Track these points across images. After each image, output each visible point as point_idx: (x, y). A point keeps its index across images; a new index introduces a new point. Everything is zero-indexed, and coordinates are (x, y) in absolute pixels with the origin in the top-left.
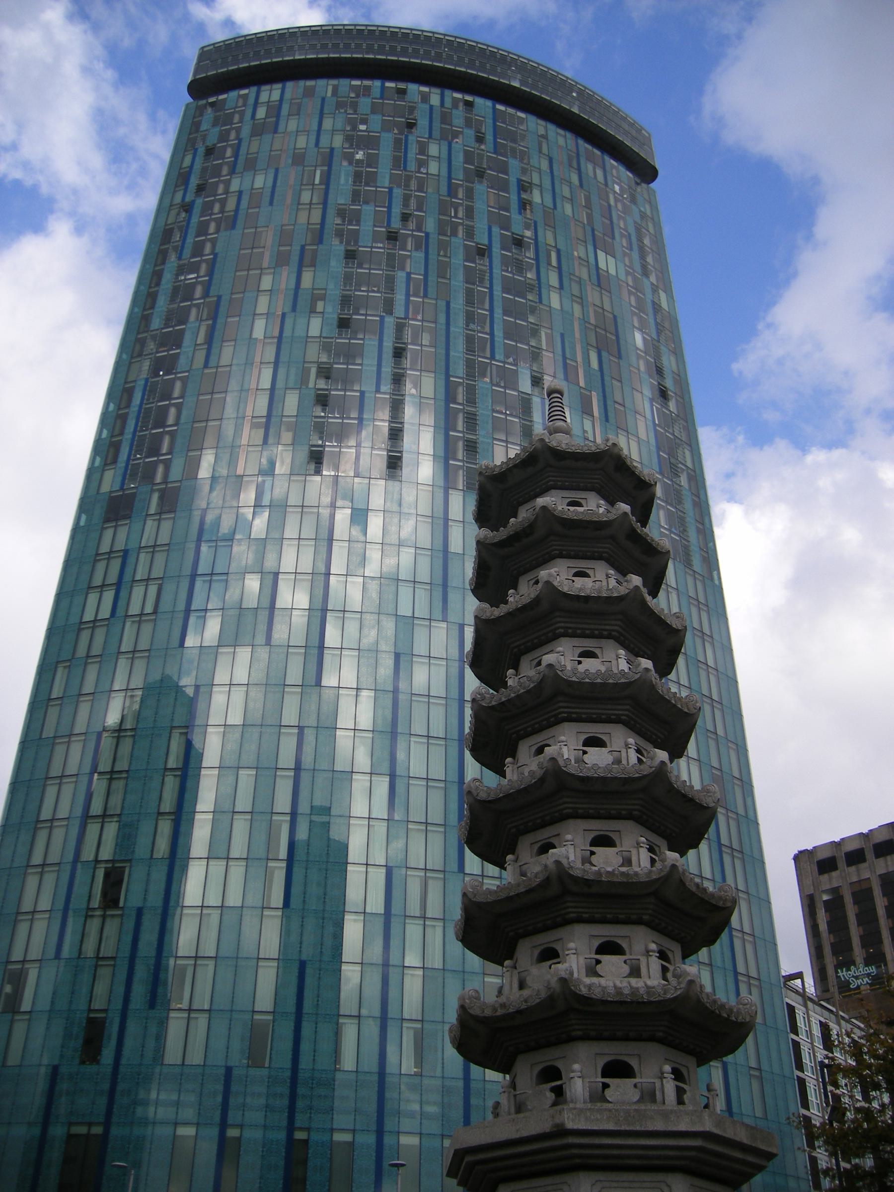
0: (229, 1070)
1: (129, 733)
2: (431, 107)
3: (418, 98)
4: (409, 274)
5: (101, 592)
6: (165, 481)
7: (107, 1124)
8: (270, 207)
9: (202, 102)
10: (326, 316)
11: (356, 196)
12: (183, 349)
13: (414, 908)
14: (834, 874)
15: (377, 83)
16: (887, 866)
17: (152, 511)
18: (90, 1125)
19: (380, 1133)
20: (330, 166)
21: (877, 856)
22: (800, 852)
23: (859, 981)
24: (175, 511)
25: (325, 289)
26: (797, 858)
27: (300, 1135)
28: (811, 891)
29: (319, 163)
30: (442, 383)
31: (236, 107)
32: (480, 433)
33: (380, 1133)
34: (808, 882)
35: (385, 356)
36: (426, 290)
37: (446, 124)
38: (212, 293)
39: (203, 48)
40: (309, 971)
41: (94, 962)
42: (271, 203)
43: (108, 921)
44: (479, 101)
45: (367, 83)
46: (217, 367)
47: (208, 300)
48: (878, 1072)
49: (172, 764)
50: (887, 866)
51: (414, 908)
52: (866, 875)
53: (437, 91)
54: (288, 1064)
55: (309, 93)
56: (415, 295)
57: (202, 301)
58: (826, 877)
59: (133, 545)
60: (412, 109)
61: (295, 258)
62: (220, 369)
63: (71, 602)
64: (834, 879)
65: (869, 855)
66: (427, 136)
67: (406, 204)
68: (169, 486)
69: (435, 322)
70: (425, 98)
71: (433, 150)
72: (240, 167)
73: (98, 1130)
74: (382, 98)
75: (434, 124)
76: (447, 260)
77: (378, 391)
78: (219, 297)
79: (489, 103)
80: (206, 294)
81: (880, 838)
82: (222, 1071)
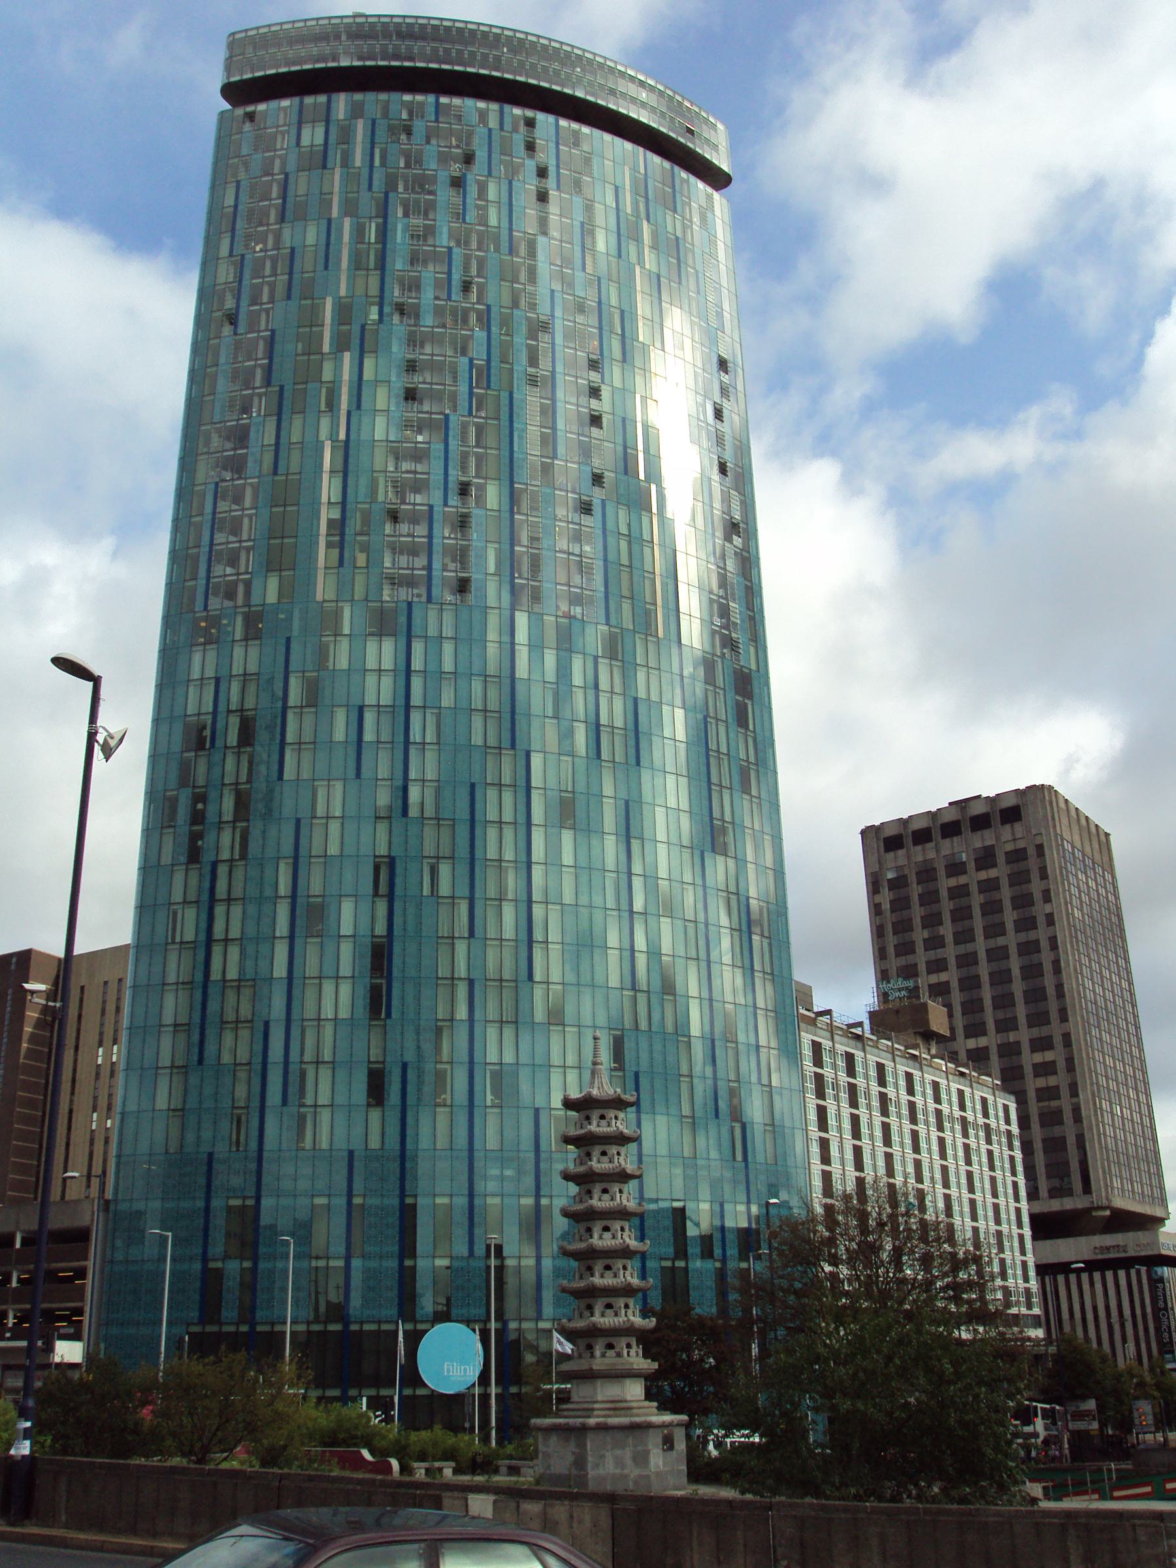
0: (351, 1153)
1: (250, 983)
2: (490, 130)
3: (475, 119)
4: (471, 360)
5: (226, 946)
6: (247, 604)
7: (258, 1199)
8: (325, 273)
9: (240, 111)
10: (391, 414)
11: (414, 259)
12: (251, 450)
13: (508, 833)
14: (901, 852)
15: (431, 98)
16: (953, 847)
17: (238, 636)
18: (244, 1198)
19: (471, 1196)
20: (385, 217)
21: (944, 836)
22: (868, 827)
23: (897, 994)
24: (260, 638)
25: (383, 1062)
26: (864, 833)
27: (409, 1201)
28: (876, 868)
29: (373, 214)
30: (506, 491)
31: (278, 126)
32: (545, 546)
33: (471, 1196)
34: (875, 858)
35: (454, 290)
36: (489, 381)
37: (505, 155)
38: (274, 382)
39: (234, 34)
40: (410, 1071)
41: (232, 1067)
42: (326, 268)
43: (207, 653)
44: (541, 117)
45: (419, 98)
46: (287, 475)
47: (270, 389)
48: (827, 1279)
49: (282, 892)
50: (953, 847)
51: (508, 833)
52: (931, 855)
53: (494, 106)
54: (398, 1147)
55: (356, 111)
56: (477, 387)
57: (263, 390)
58: (891, 855)
59: (224, 673)
60: (470, 135)
61: (355, 342)
62: (290, 477)
63: (172, 711)
64: (899, 857)
65: (936, 834)
66: (486, 173)
67: (466, 268)
68: (253, 609)
69: (499, 449)
70: (483, 116)
71: (492, 193)
72: (289, 214)
73: (250, 1202)
74: (437, 121)
75: (493, 156)
76: (508, 338)
77: (446, 504)
78: (282, 388)
79: (551, 118)
80: (268, 382)
81: (947, 818)
82: (346, 1154)
